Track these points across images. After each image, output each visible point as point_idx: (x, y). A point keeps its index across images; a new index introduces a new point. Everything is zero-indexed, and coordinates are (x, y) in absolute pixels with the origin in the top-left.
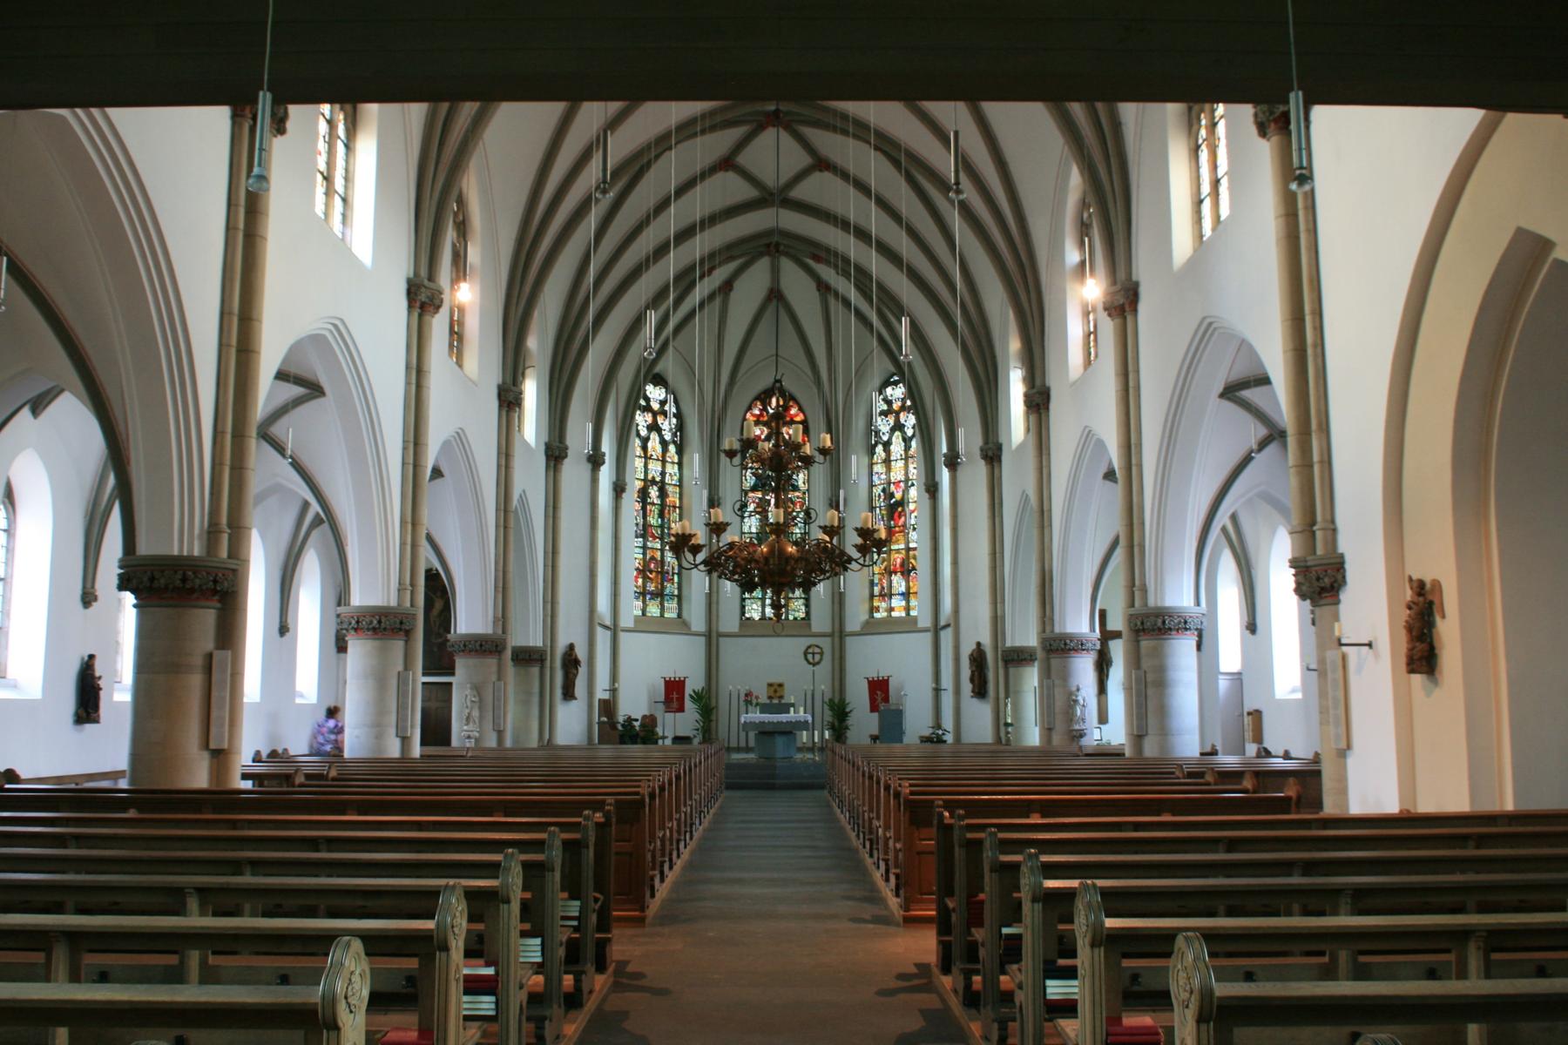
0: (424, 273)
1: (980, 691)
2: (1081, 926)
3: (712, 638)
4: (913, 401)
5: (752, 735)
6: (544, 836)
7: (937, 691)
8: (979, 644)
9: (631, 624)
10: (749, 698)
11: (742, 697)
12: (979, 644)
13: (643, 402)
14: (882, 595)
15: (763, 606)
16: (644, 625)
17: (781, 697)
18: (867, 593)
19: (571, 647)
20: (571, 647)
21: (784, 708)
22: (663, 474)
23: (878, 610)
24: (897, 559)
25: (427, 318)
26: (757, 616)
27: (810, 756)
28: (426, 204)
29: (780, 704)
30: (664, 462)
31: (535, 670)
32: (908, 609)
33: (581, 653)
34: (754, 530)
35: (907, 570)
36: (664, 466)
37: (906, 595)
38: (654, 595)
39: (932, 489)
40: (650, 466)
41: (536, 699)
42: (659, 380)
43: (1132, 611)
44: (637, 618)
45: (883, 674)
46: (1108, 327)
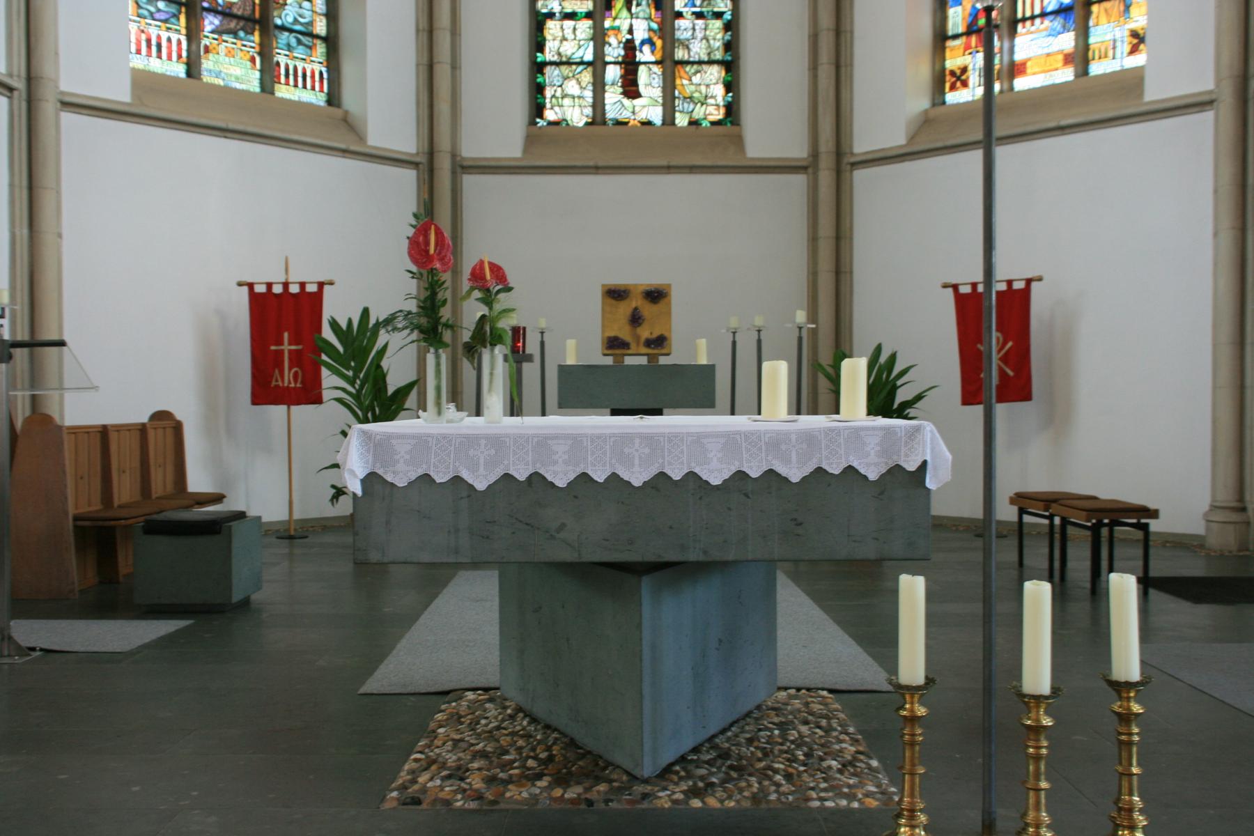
3: (438, 171)
15: (599, 86)
17: (659, 342)
23: (960, 78)
26: (578, 116)
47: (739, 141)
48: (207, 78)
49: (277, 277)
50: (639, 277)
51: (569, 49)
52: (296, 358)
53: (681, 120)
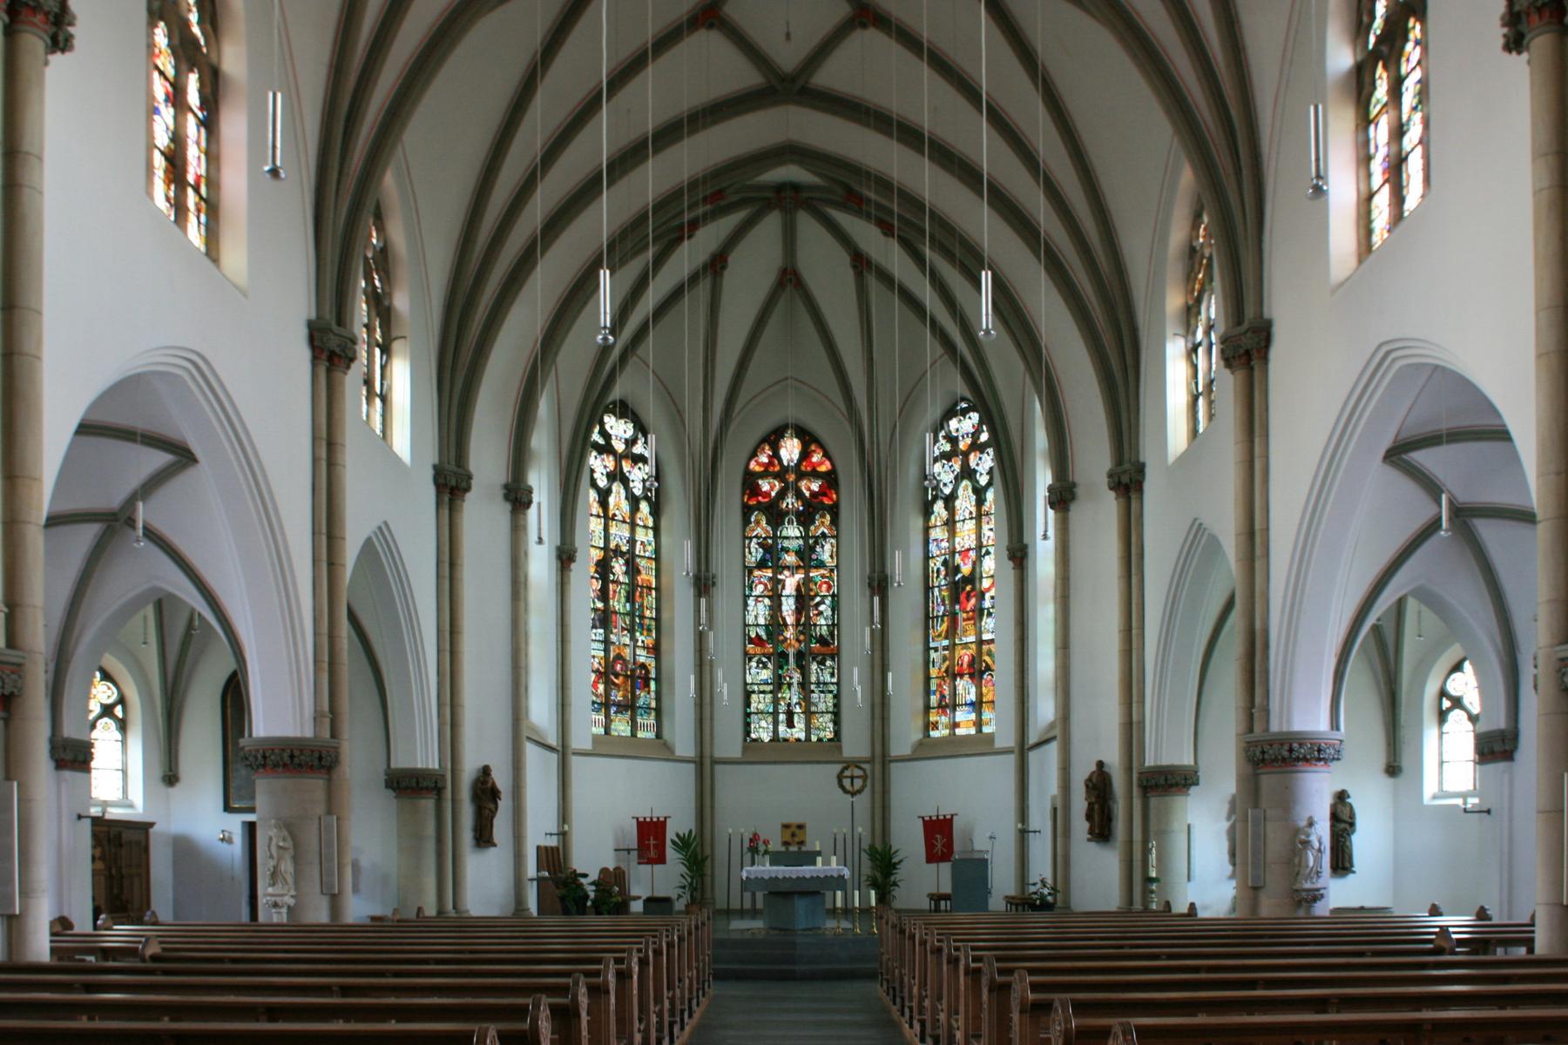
0: (329, 316)
1: (1101, 831)
2: (985, 981)
3: (704, 766)
4: (992, 431)
5: (760, 896)
6: (570, 980)
7: (1023, 834)
8: (1100, 764)
9: (587, 745)
10: (754, 847)
11: (746, 844)
12: (1100, 764)
13: (596, 437)
14: (942, 707)
15: (776, 723)
16: (606, 747)
17: (802, 843)
18: (920, 704)
19: (486, 771)
20: (486, 771)
21: (810, 858)
22: (632, 541)
23: (935, 726)
24: (965, 656)
25: (338, 374)
26: (766, 737)
27: (846, 924)
28: (329, 214)
29: (800, 852)
31: (428, 804)
32: (979, 724)
33: (501, 779)
34: (762, 621)
35: (977, 671)
36: (633, 531)
37: (977, 706)
38: (622, 707)
39: (1019, 554)
40: (613, 530)
41: (430, 846)
42: (624, 410)
43: (1251, 737)
44: (596, 739)
45: (946, 811)
46: (1229, 384)
47: (840, 748)
48: (614, 733)
49: (648, 815)
50: (795, 820)
51: (761, 707)
52: (656, 846)
53: (814, 738)
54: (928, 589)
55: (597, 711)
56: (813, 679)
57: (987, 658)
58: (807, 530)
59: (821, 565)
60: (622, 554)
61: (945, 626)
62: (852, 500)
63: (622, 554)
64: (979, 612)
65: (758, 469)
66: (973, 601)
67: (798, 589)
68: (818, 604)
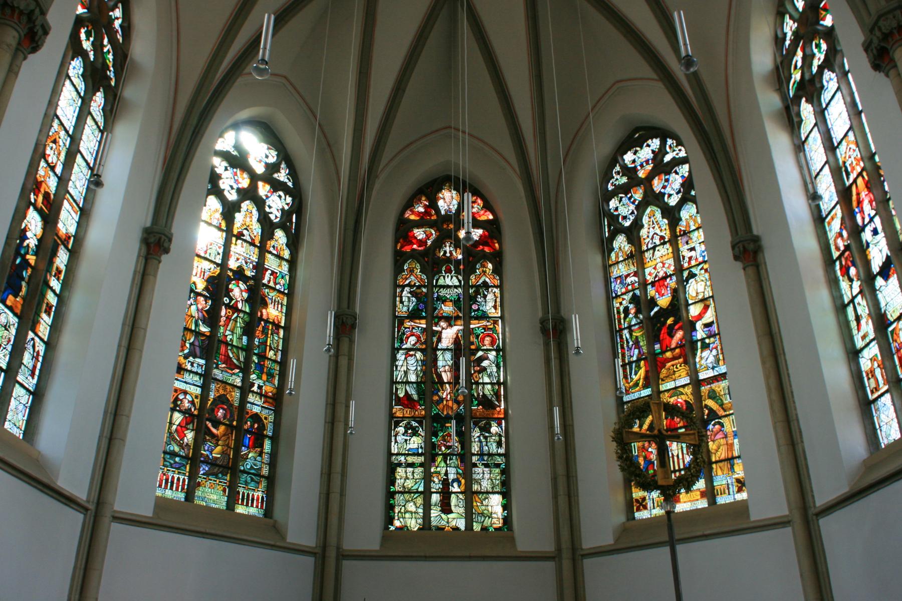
15: (427, 506)
22: (260, 267)
23: (642, 504)
26: (414, 524)
30: (263, 250)
34: (412, 378)
36: (262, 257)
47: (512, 540)
51: (409, 484)
53: (477, 527)
54: (614, 332)
55: (179, 467)
56: (475, 448)
57: (710, 403)
58: (467, 279)
59: (484, 316)
60: (245, 279)
61: (642, 372)
62: (518, 245)
63: (245, 279)
64: (689, 349)
65: (413, 217)
66: (679, 334)
67: (456, 341)
68: (482, 359)
